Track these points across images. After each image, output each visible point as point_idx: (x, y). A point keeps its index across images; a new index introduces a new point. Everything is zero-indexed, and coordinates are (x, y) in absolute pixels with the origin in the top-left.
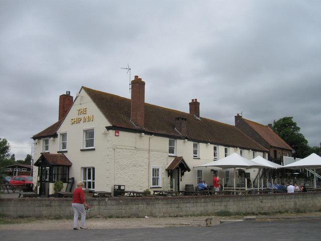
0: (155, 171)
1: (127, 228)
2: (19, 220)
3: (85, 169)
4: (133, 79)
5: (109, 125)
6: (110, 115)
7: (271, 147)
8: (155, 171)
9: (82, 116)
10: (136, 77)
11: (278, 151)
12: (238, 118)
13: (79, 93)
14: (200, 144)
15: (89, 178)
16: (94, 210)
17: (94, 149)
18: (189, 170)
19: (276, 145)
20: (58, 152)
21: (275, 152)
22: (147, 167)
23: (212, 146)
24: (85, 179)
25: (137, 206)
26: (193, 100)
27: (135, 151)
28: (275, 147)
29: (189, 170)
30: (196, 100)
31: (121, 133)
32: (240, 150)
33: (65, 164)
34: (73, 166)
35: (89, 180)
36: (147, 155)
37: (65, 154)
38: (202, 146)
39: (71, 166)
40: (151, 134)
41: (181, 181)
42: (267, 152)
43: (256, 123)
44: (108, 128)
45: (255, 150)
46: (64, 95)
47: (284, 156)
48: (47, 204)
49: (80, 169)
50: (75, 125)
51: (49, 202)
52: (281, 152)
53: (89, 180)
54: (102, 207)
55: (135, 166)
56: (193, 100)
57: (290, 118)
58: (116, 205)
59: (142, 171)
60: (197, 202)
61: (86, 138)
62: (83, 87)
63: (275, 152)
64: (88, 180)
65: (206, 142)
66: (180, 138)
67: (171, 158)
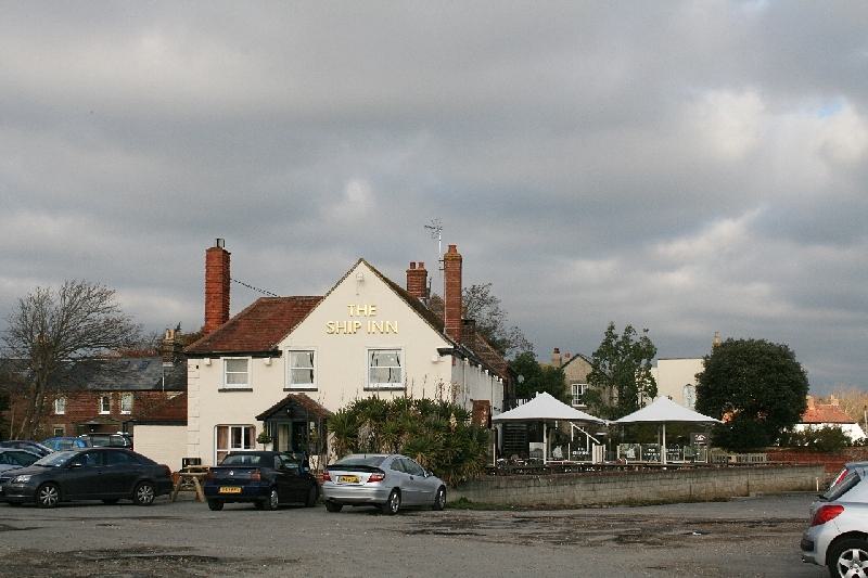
5: (446, 345)
44: (442, 352)
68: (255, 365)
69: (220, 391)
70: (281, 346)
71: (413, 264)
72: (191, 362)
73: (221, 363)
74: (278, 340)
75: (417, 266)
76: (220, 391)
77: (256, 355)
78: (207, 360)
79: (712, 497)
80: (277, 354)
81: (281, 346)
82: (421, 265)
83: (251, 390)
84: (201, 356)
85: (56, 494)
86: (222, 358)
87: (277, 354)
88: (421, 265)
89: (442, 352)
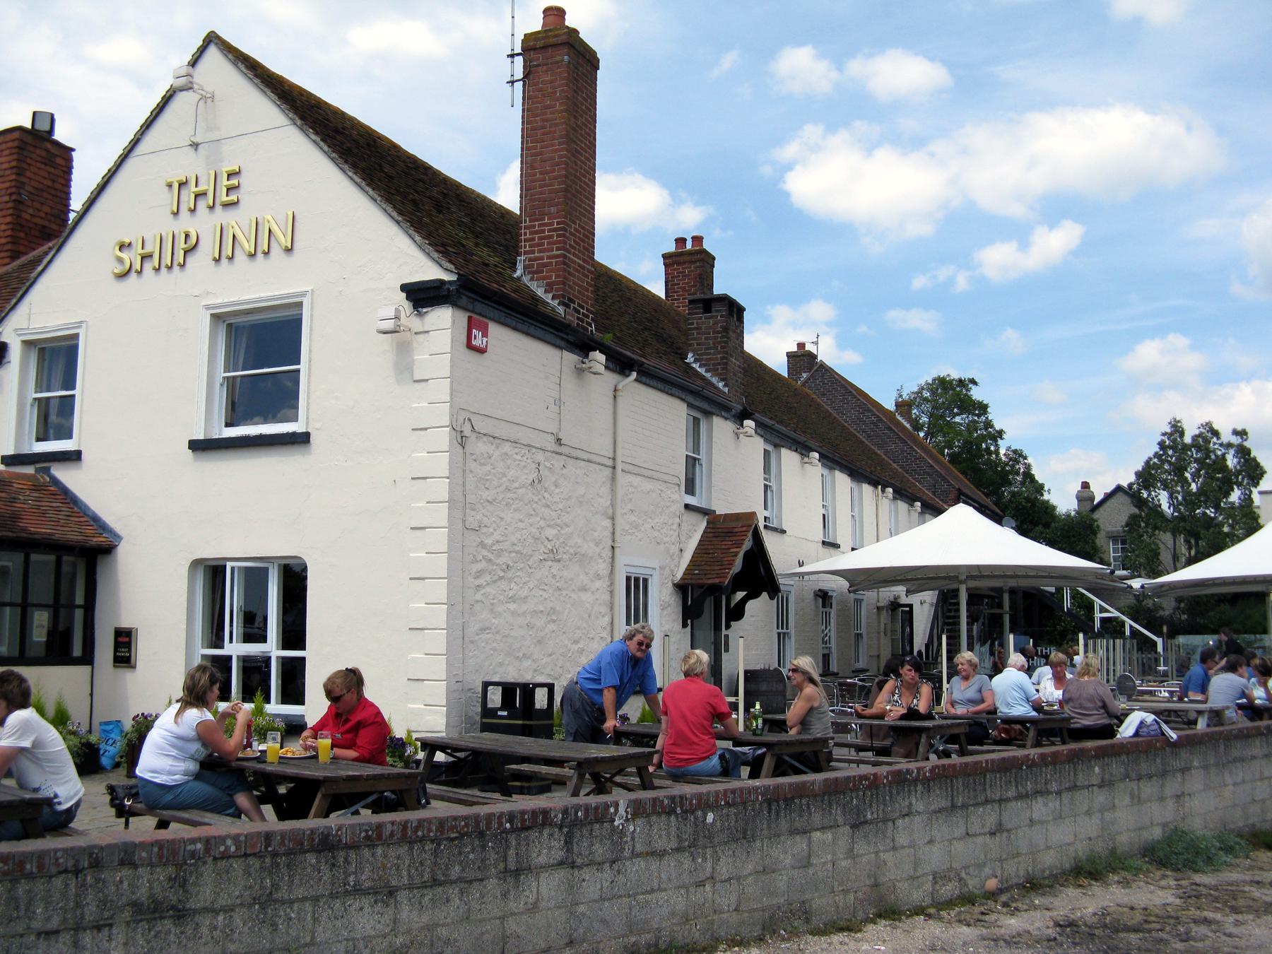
0: (637, 587)
3: (214, 573)
4: (535, 24)
5: (429, 270)
8: (637, 587)
9: (204, 225)
10: (555, 14)
13: (194, 63)
15: (254, 630)
16: (534, 908)
17: (302, 439)
22: (602, 567)
24: (217, 641)
25: (800, 844)
26: (681, 241)
27: (558, 462)
30: (698, 240)
31: (500, 338)
33: (71, 534)
34: (122, 551)
35: (254, 649)
36: (605, 490)
37: (65, 475)
39: (108, 550)
41: (727, 650)
46: (20, 129)
48: (142, 894)
49: (1204, 420)
50: (149, 283)
51: (162, 874)
53: (254, 649)
54: (594, 883)
55: (553, 555)
56: (681, 241)
57: (961, 382)
58: (679, 850)
59: (584, 589)
60: (1074, 788)
61: (229, 365)
62: (212, 39)
64: (235, 649)
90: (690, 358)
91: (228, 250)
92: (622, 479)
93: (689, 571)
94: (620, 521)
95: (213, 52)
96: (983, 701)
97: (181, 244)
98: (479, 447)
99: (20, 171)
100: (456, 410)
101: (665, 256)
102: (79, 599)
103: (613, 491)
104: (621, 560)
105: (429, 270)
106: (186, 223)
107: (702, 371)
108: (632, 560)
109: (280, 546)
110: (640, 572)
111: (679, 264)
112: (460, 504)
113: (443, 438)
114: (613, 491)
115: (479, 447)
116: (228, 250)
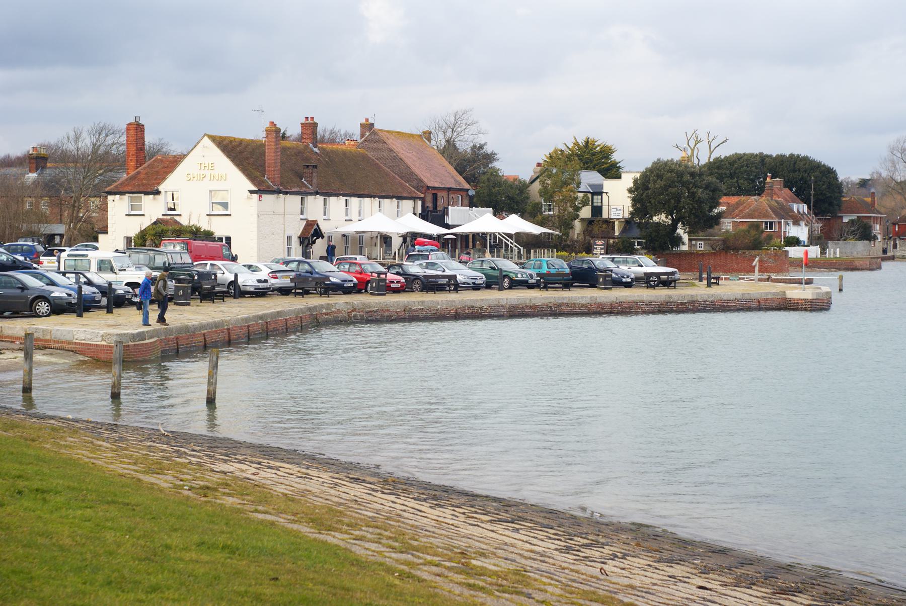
0: (289, 238)
1: (402, 324)
2: (337, 324)
5: (254, 188)
6: (893, 163)
7: (428, 188)
8: (289, 238)
9: (208, 173)
11: (442, 196)
12: (368, 127)
14: (331, 198)
18: (323, 237)
19: (437, 185)
20: (163, 215)
21: (435, 196)
22: (282, 235)
23: (322, 198)
28: (434, 188)
29: (323, 237)
32: (397, 201)
38: (332, 200)
40: (286, 193)
42: (420, 198)
43: (399, 133)
44: (251, 192)
45: (400, 198)
47: (449, 207)
52: (445, 195)
62: (205, 135)
63: (435, 196)
65: (337, 195)
66: (311, 194)
67: (302, 221)
68: (147, 200)
69: (126, 215)
70: (161, 188)
71: (307, 118)
72: (110, 198)
73: (126, 197)
74: (159, 184)
75: (309, 119)
76: (126, 215)
77: (146, 193)
78: (117, 196)
79: (755, 305)
80: (158, 193)
81: (161, 188)
82: (312, 118)
83: (230, 215)
84: (115, 194)
85: (43, 303)
86: (127, 195)
87: (158, 193)
88: (312, 118)
89: (251, 192)
90: (303, 179)
91: (212, 179)
92: (286, 216)
93: (301, 234)
94: (286, 225)
95: (206, 137)
96: (174, 209)
97: (202, 176)
98: (261, 217)
99: (137, 135)
100: (258, 211)
101: (302, 124)
102: (14, 247)
103: (284, 219)
104: (286, 233)
105: (254, 188)
106: (202, 172)
107: (306, 183)
108: (288, 233)
109: (228, 235)
110: (290, 235)
111: (306, 126)
112: (259, 227)
113: (256, 216)
114: (284, 219)
115: (261, 217)
116: (212, 179)
